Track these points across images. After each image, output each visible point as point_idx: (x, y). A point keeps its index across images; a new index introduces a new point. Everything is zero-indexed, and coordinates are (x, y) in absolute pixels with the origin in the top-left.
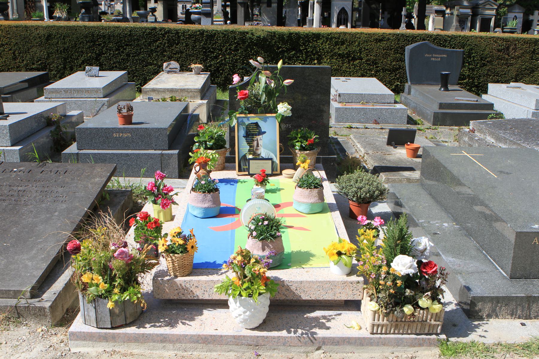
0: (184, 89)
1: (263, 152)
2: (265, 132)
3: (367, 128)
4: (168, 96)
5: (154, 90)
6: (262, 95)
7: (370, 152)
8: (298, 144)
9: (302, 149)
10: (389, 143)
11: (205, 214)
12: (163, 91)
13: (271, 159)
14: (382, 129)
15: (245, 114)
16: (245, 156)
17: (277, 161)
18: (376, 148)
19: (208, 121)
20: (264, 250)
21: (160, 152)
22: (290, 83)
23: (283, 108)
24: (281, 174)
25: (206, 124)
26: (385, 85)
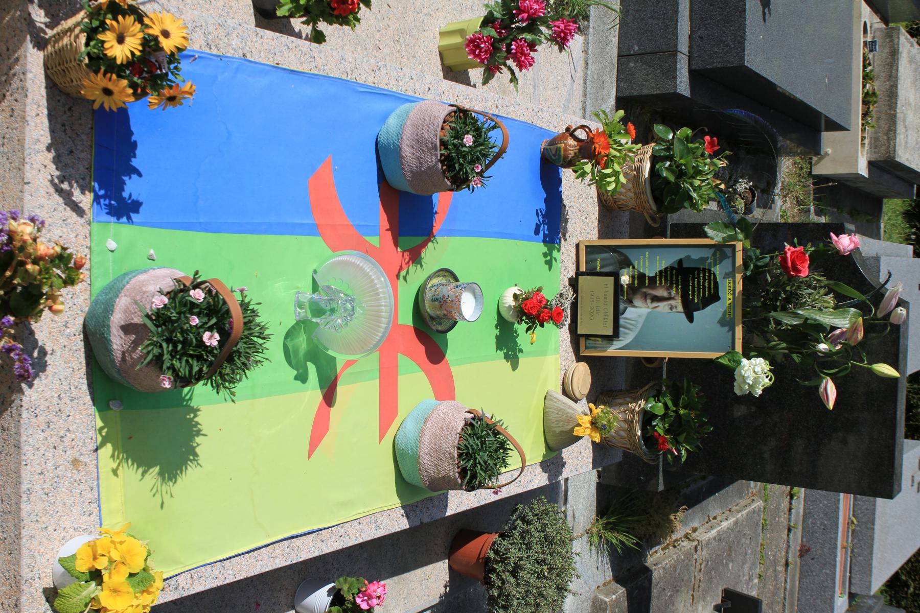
0: (894, 123)
1: (637, 313)
2: (691, 319)
3: (789, 530)
4: (877, 86)
5: (894, 54)
6: (796, 316)
7: (704, 554)
8: (659, 409)
9: (647, 418)
10: (729, 595)
11: (387, 147)
12: (890, 76)
13: (616, 334)
14: (787, 564)
15: (746, 265)
16: (627, 263)
17: (613, 350)
18: (716, 565)
19: (815, 177)
20: (127, 329)
21: (683, 45)
22: (824, 398)
23: (755, 373)
24: (579, 358)
25: (810, 174)
26: (909, 561)
